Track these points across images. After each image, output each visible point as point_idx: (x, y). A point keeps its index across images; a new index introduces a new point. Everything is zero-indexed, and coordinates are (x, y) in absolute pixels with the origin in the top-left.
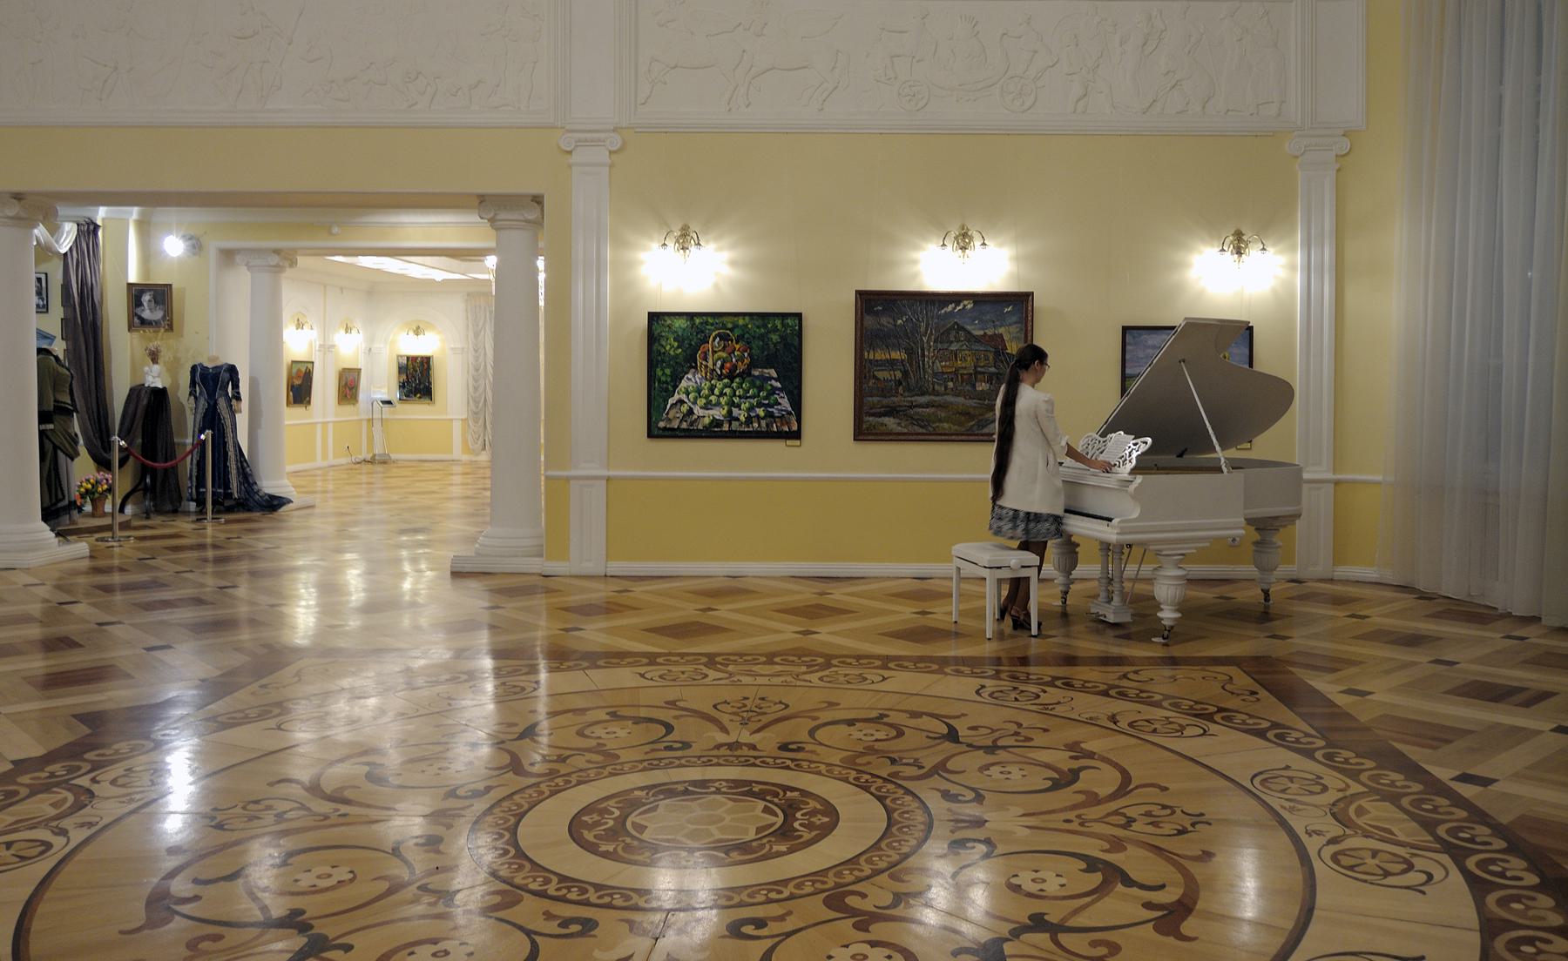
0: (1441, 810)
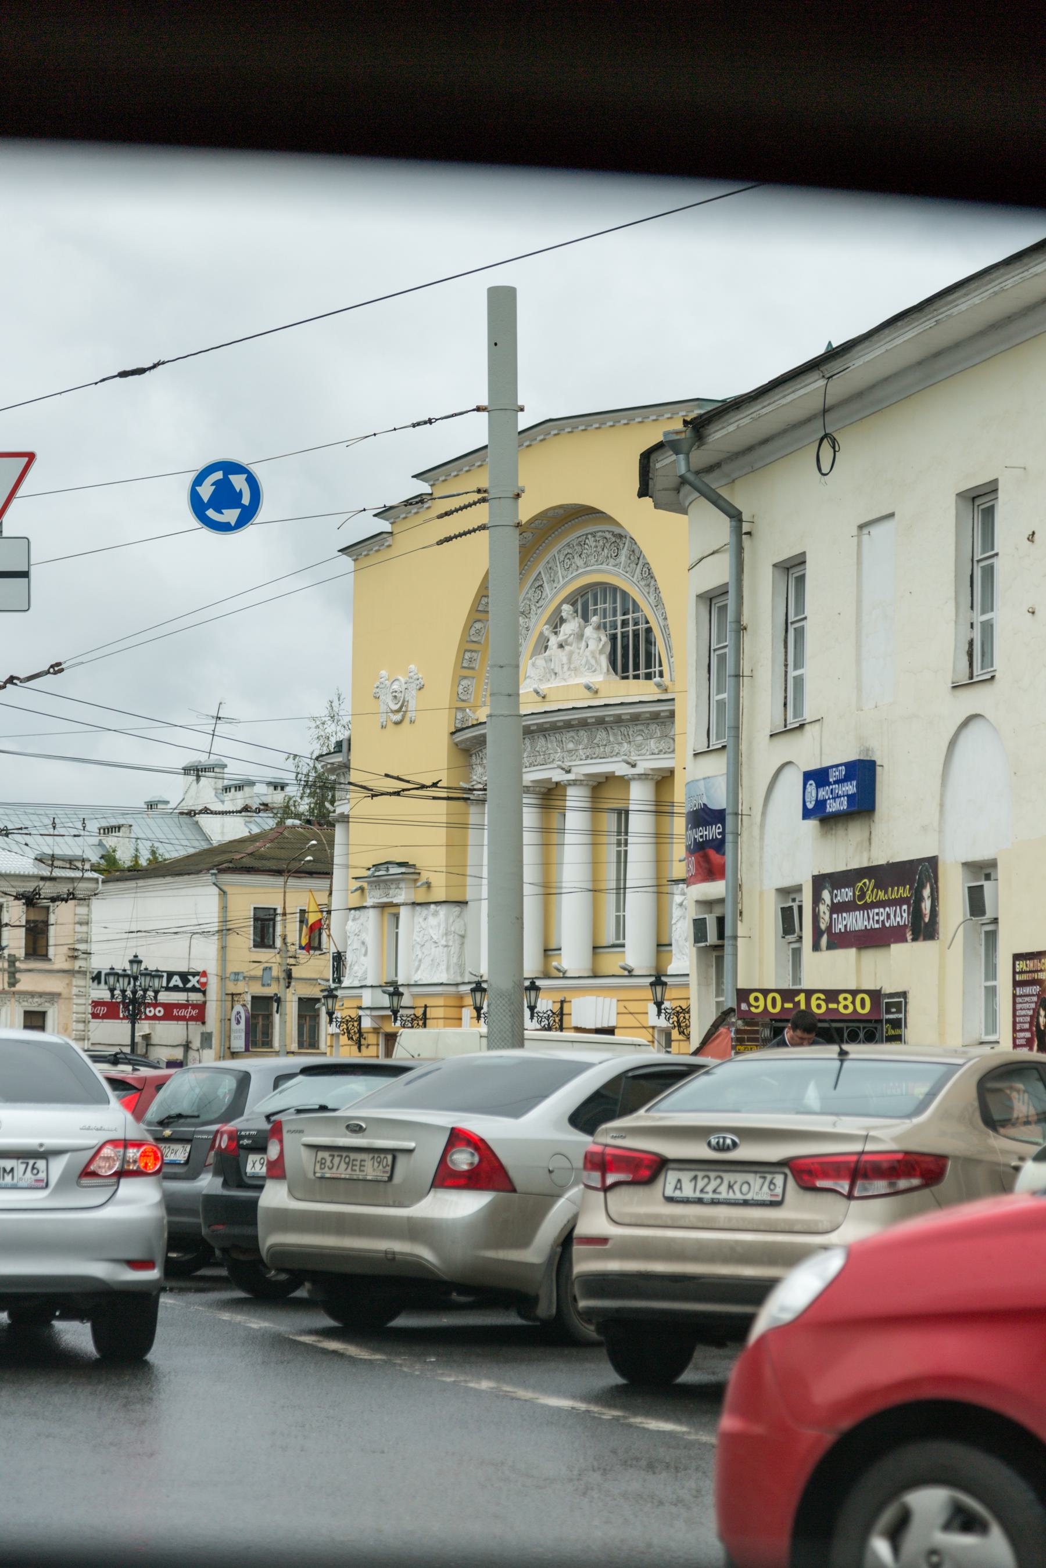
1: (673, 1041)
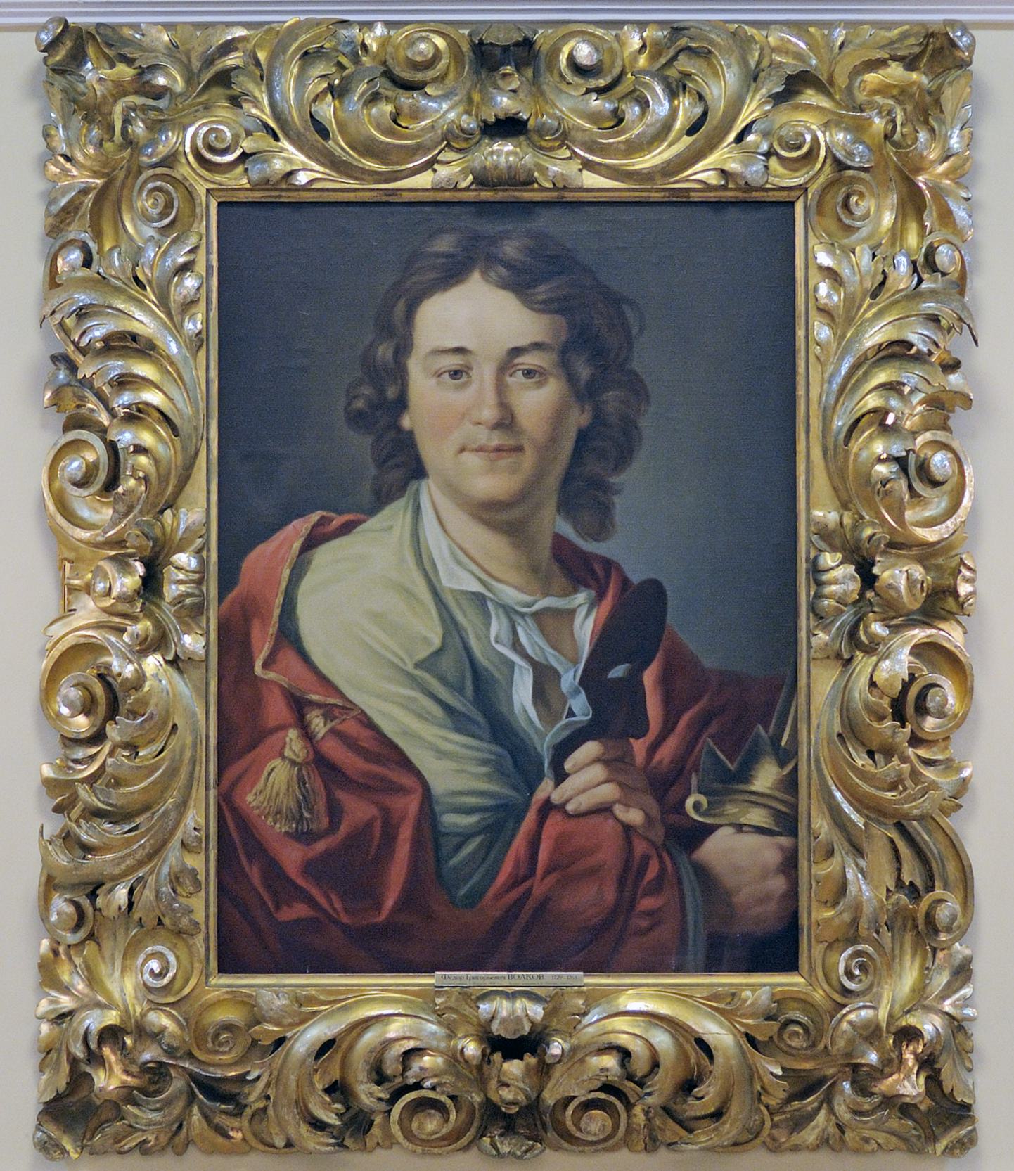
0: (200, 107)
1: (171, 563)
